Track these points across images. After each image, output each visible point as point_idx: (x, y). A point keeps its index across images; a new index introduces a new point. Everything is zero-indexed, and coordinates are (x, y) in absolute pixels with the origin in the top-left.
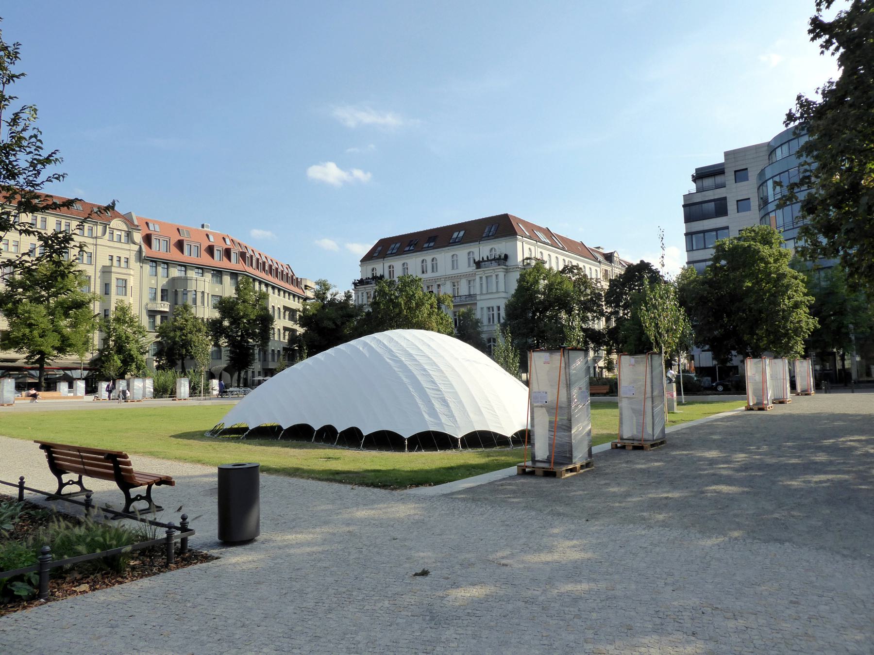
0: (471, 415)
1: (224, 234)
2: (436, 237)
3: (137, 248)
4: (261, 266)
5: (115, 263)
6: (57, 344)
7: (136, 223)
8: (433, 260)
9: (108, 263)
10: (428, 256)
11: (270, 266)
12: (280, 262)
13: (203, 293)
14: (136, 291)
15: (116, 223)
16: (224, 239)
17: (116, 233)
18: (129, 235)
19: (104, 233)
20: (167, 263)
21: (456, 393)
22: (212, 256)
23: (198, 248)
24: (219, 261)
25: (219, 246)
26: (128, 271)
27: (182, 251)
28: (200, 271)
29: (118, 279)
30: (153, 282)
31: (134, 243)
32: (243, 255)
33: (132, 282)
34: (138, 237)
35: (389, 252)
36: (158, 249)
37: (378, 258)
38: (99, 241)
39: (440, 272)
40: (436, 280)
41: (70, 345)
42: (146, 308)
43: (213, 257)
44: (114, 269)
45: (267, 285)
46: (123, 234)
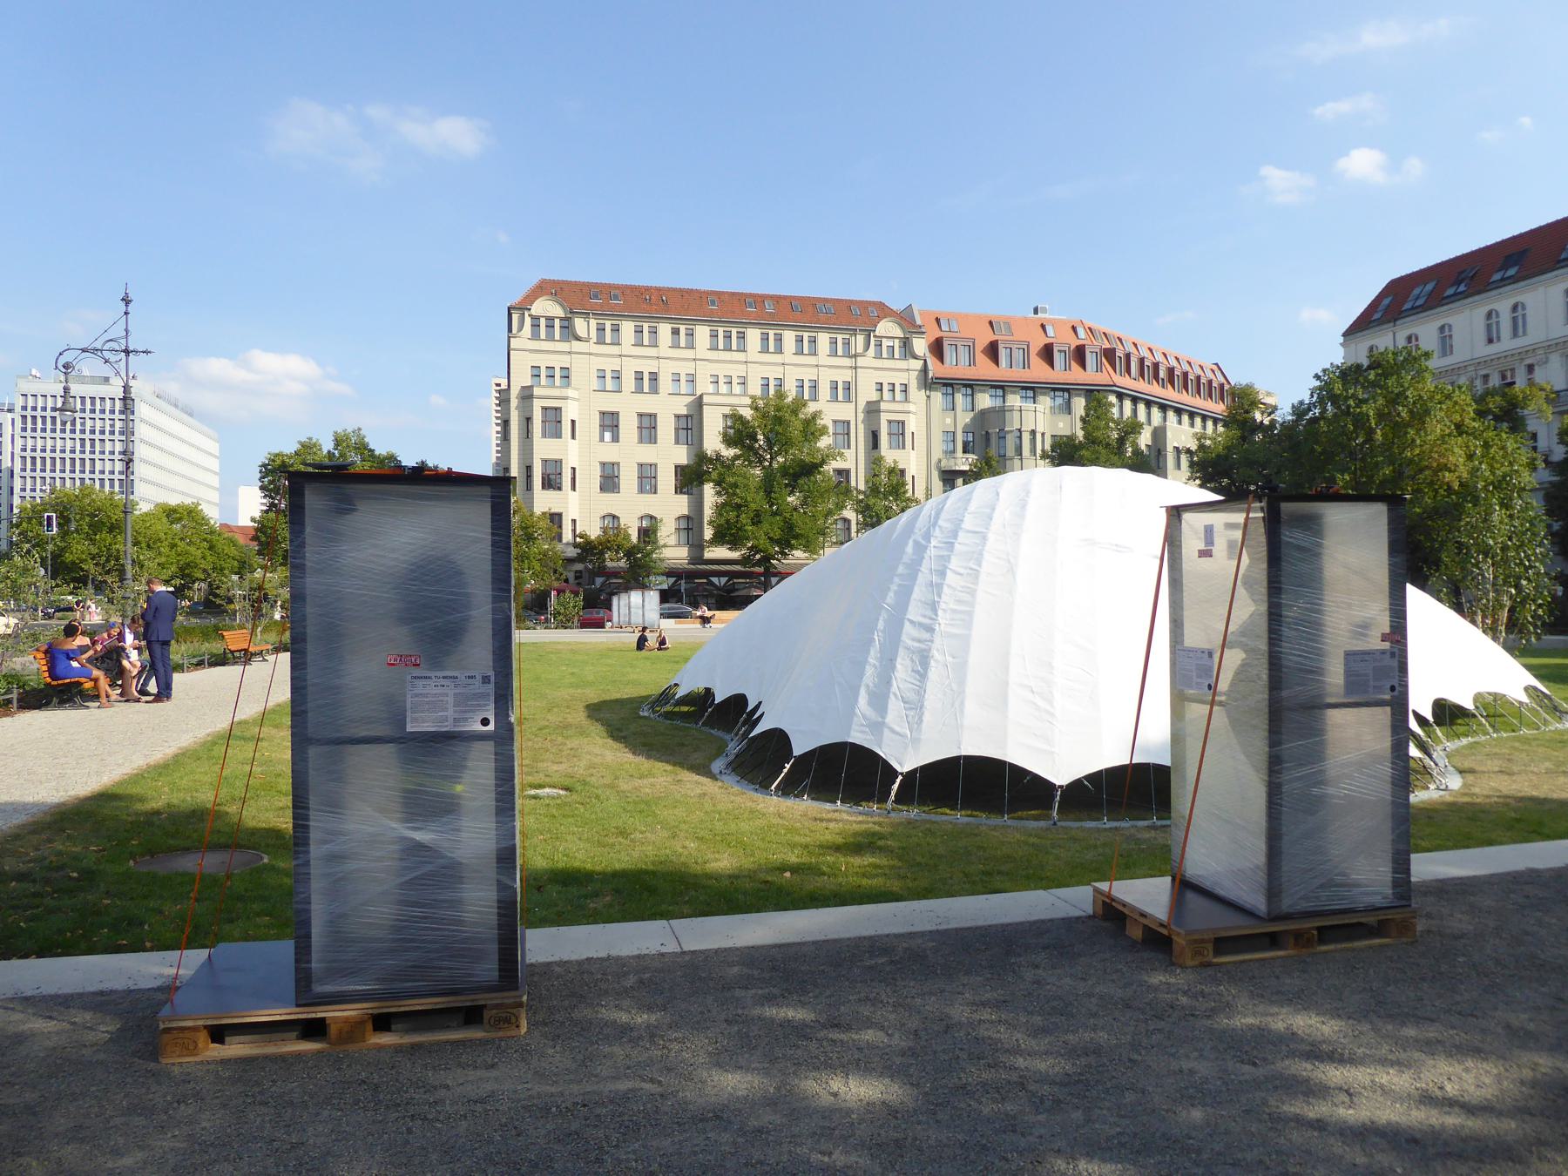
0: (971, 707)
1: (1074, 318)
2: (1524, 252)
3: (918, 364)
4: (1150, 370)
5: (887, 395)
6: (777, 534)
7: (919, 322)
8: (1515, 308)
9: (874, 396)
10: (1502, 302)
11: (1171, 371)
12: (1197, 359)
13: (1033, 432)
14: (921, 441)
15: (887, 328)
16: (1074, 328)
17: (886, 343)
18: (906, 344)
19: (867, 347)
20: (971, 386)
21: (965, 640)
22: (1051, 363)
23: (1026, 352)
24: (1062, 372)
25: (1065, 341)
26: (905, 407)
27: (996, 360)
28: (1030, 394)
29: (890, 422)
30: (949, 421)
31: (915, 357)
32: (1109, 354)
33: (914, 425)
34: (920, 345)
35: (1408, 306)
36: (956, 365)
37: (1381, 322)
38: (861, 361)
39: (1536, 333)
40: (1522, 354)
41: (796, 537)
42: (939, 468)
43: (1052, 366)
44: (883, 406)
45: (1164, 408)
46: (897, 343)
